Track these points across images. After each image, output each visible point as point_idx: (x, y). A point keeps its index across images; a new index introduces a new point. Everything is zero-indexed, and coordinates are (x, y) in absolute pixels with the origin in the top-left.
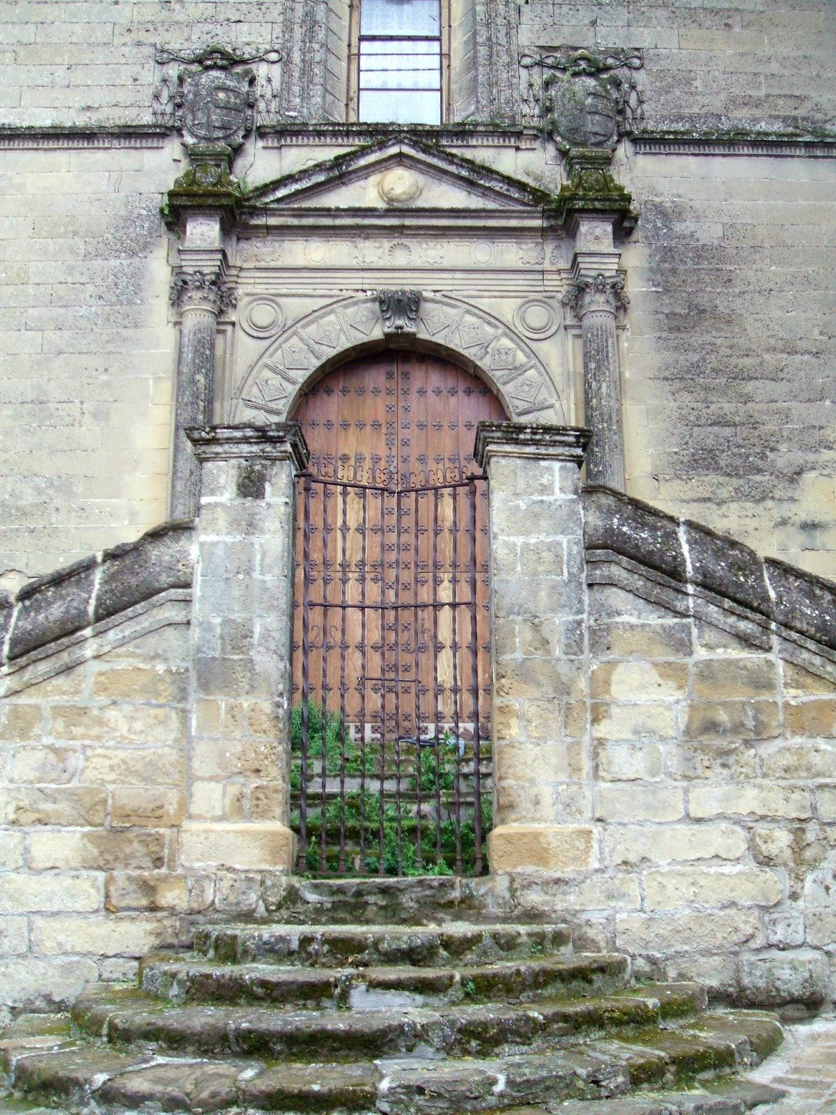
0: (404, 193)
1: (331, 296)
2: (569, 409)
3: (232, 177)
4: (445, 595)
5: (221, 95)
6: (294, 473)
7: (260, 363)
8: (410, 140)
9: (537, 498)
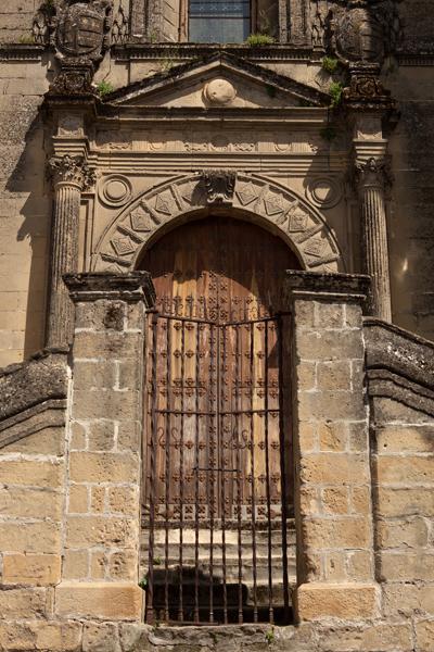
0: (224, 97)
1: (167, 176)
2: (349, 262)
3: (93, 84)
4: (258, 404)
5: (85, 21)
6: (145, 310)
7: (114, 226)
8: (228, 56)
9: (329, 329)
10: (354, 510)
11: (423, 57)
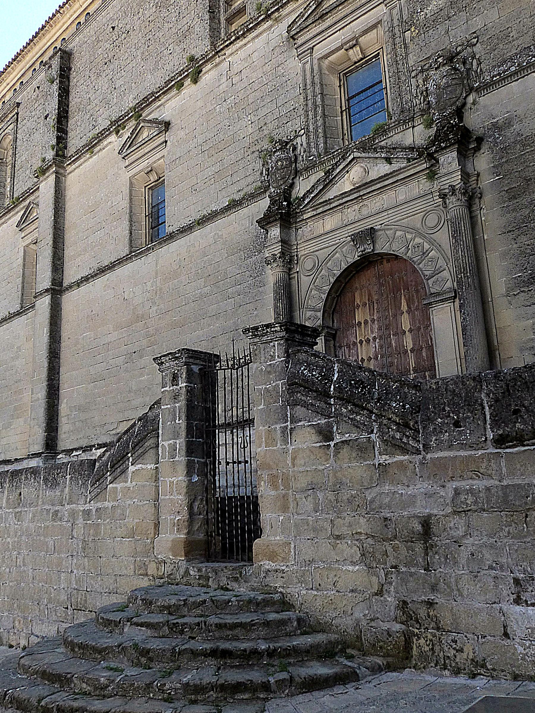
10: (282, 488)
11: (498, 82)
